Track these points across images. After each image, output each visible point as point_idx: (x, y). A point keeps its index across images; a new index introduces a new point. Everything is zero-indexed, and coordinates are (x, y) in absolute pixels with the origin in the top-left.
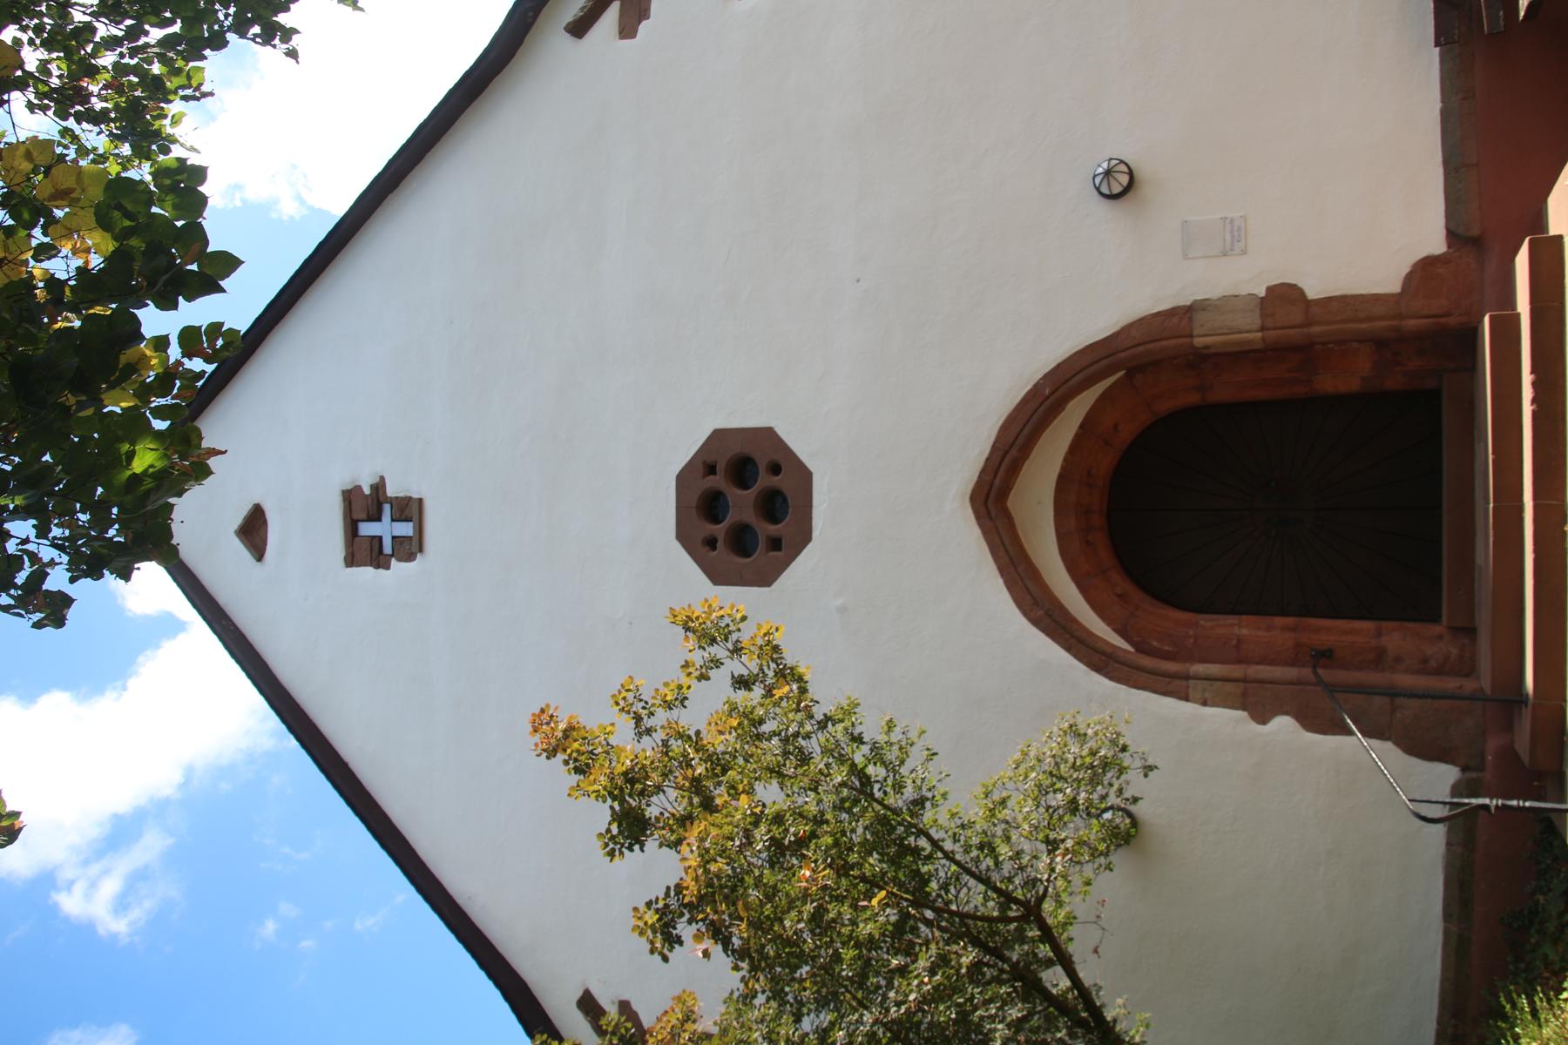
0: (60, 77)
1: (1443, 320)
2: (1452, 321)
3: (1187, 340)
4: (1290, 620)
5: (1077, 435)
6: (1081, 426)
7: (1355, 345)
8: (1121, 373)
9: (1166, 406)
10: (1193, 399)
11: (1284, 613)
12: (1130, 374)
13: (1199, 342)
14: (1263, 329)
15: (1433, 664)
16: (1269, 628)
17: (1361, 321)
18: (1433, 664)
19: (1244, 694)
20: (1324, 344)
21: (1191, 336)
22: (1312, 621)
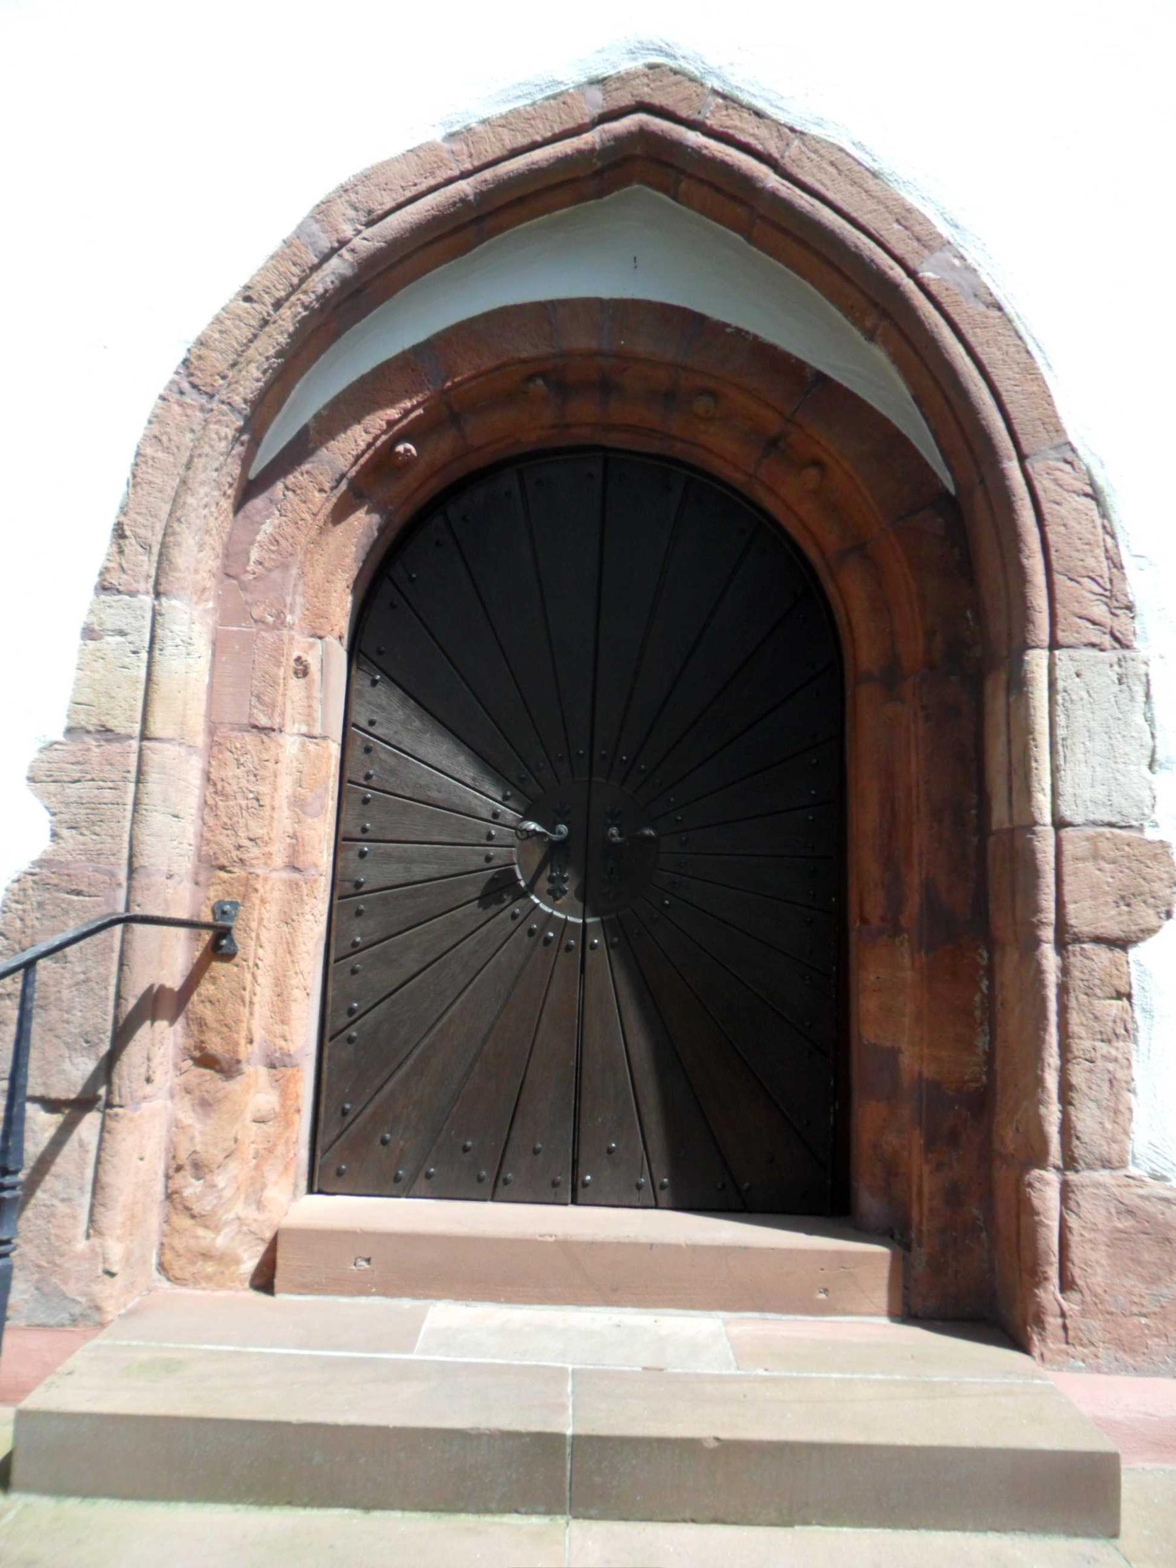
0: (613, 835)
1: (1053, 1272)
2: (1050, 1294)
3: (1042, 632)
4: (324, 859)
5: (801, 365)
6: (821, 377)
7: (982, 1042)
8: (947, 480)
9: (852, 596)
10: (865, 653)
11: (342, 840)
12: (953, 509)
13: (1037, 661)
14: (1059, 824)
15: (192, 1188)
16: (298, 804)
17: (1063, 1072)
18: (192, 1188)
19: (106, 732)
20: (990, 972)
21: (1054, 645)
22: (321, 906)
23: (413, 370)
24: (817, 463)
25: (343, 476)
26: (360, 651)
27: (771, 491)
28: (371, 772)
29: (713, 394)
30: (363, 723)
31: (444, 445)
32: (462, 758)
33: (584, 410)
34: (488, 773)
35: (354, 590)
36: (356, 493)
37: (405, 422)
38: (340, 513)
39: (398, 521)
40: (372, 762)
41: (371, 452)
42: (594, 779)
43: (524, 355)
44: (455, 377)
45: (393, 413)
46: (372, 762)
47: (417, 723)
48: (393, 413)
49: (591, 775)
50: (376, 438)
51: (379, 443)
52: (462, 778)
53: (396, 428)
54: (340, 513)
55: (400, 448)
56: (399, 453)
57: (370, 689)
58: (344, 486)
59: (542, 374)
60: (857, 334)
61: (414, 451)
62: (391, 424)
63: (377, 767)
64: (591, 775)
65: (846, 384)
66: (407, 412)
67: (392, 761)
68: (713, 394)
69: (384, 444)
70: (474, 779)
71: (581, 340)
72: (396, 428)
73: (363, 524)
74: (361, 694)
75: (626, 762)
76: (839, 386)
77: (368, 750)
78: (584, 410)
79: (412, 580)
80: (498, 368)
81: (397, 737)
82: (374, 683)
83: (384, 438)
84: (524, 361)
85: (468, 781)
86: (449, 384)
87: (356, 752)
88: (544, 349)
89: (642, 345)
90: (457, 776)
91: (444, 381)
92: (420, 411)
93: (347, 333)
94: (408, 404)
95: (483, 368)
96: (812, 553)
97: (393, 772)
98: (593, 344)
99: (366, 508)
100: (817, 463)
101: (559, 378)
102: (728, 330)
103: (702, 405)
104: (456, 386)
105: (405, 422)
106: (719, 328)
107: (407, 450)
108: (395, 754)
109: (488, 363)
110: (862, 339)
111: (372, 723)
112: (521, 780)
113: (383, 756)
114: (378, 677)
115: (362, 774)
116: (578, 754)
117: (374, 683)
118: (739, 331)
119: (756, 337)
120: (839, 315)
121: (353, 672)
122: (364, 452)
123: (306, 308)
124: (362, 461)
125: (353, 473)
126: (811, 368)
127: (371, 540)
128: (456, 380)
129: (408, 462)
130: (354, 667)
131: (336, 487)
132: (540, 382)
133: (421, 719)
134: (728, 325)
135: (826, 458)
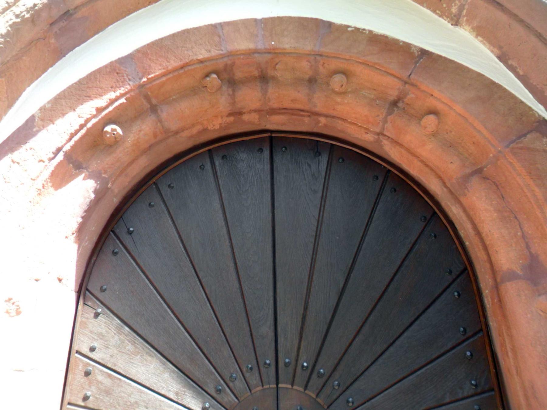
6: (424, 53)
23: (117, 73)
24: (434, 112)
25: (59, 150)
26: (87, 290)
27: (396, 143)
28: (89, 393)
29: (344, 73)
30: (85, 350)
31: (144, 129)
32: (166, 375)
33: (250, 97)
34: (190, 387)
35: (76, 242)
36: (74, 161)
37: (111, 109)
38: (60, 178)
39: (119, 188)
40: (90, 383)
41: (83, 131)
42: (280, 385)
43: (200, 57)
44: (149, 75)
45: (101, 102)
46: (90, 383)
47: (130, 347)
48: (101, 102)
49: (277, 384)
50: (87, 121)
51: (89, 125)
52: (167, 394)
53: (103, 114)
54: (60, 178)
55: (108, 129)
56: (106, 132)
57: (93, 320)
58: (60, 157)
59: (215, 72)
60: (445, 23)
61: (119, 131)
62: (99, 110)
63: (93, 388)
64: (277, 384)
65: (444, 55)
66: (112, 102)
67: (107, 382)
68: (344, 73)
69: (94, 125)
70: (177, 394)
71: (243, 44)
72: (103, 114)
73: (82, 190)
74: (84, 325)
75: (307, 367)
76: (440, 56)
77: (87, 374)
78: (250, 97)
79: (130, 233)
80: (182, 67)
81: (113, 360)
82: (97, 315)
83: (94, 121)
84: (201, 62)
85: (172, 396)
86: (145, 79)
87: (77, 377)
88: (214, 52)
89: (288, 43)
90: (163, 392)
91: (141, 79)
92: (123, 100)
93: (71, 53)
94: (112, 95)
95: (170, 68)
96: (434, 186)
97: (108, 392)
98: (252, 46)
99: (83, 175)
100: (434, 112)
101: (227, 74)
102: (349, 29)
103: (338, 79)
104: (150, 81)
105: (111, 109)
106: (343, 29)
107: (113, 130)
108: (110, 376)
109: (174, 63)
110: (449, 25)
111: (92, 349)
112: (219, 391)
113: (100, 378)
114: (99, 310)
115: (81, 396)
116: (265, 363)
117: (97, 315)
118: (357, 30)
119: (370, 32)
120: (428, 12)
121: (80, 307)
122: (77, 132)
123: (17, 16)
124: (76, 138)
125: (67, 147)
126: (415, 47)
127: (88, 200)
128: (150, 76)
129: (117, 141)
130: (81, 303)
131: (53, 158)
132: (214, 76)
133: (133, 343)
134: (349, 27)
135: (440, 106)
